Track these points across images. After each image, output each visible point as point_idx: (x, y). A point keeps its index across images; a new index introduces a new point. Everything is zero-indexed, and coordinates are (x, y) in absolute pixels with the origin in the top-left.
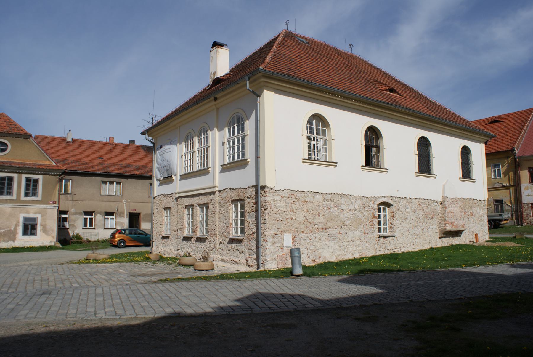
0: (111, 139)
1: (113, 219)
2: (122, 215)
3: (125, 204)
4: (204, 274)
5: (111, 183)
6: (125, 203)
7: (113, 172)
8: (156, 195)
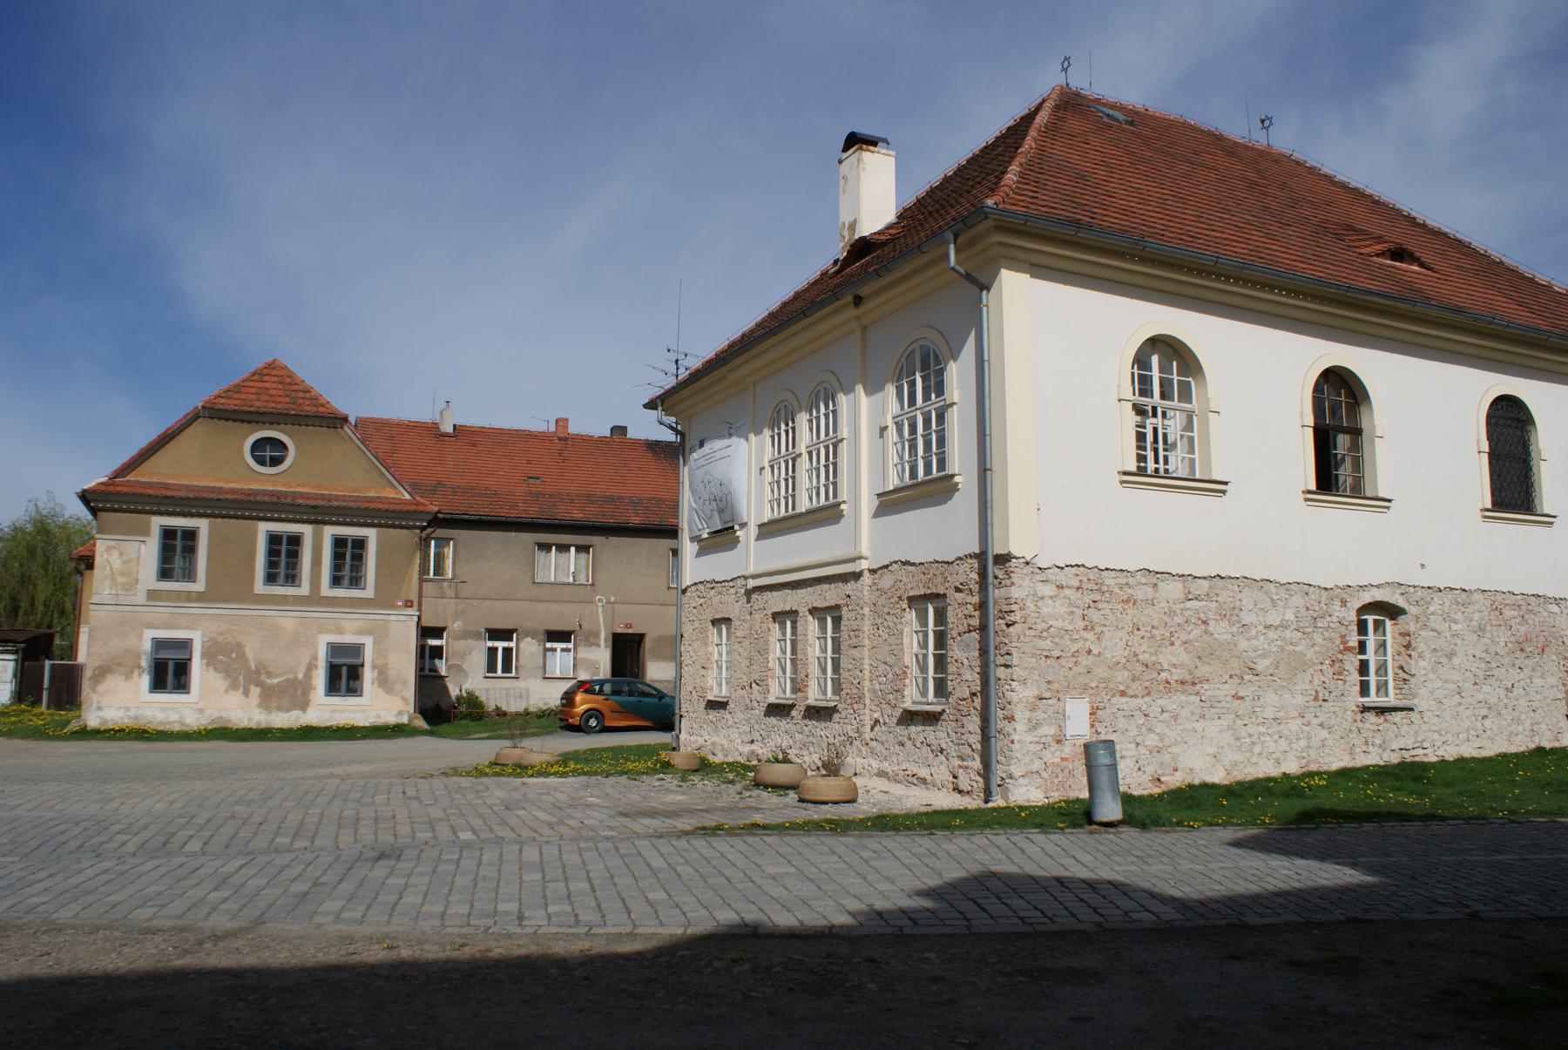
0: (561, 422)
1: (568, 650)
2: (592, 640)
3: (600, 609)
5: (563, 548)
6: (600, 604)
7: (568, 516)
8: (689, 584)
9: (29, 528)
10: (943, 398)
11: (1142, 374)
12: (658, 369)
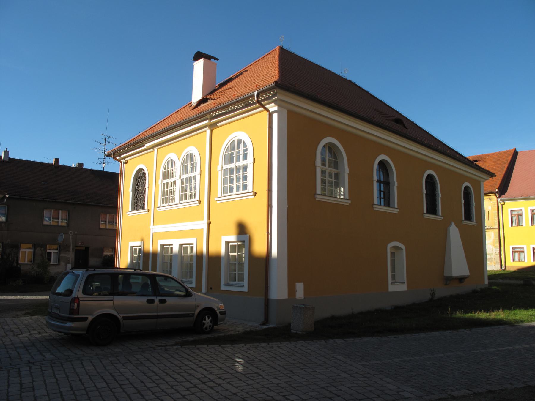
0: (81, 165)
3: (71, 237)
4: (257, 328)
6: (71, 234)
9: (483, 311)
10: (246, 172)
11: (335, 161)
12: (97, 142)
